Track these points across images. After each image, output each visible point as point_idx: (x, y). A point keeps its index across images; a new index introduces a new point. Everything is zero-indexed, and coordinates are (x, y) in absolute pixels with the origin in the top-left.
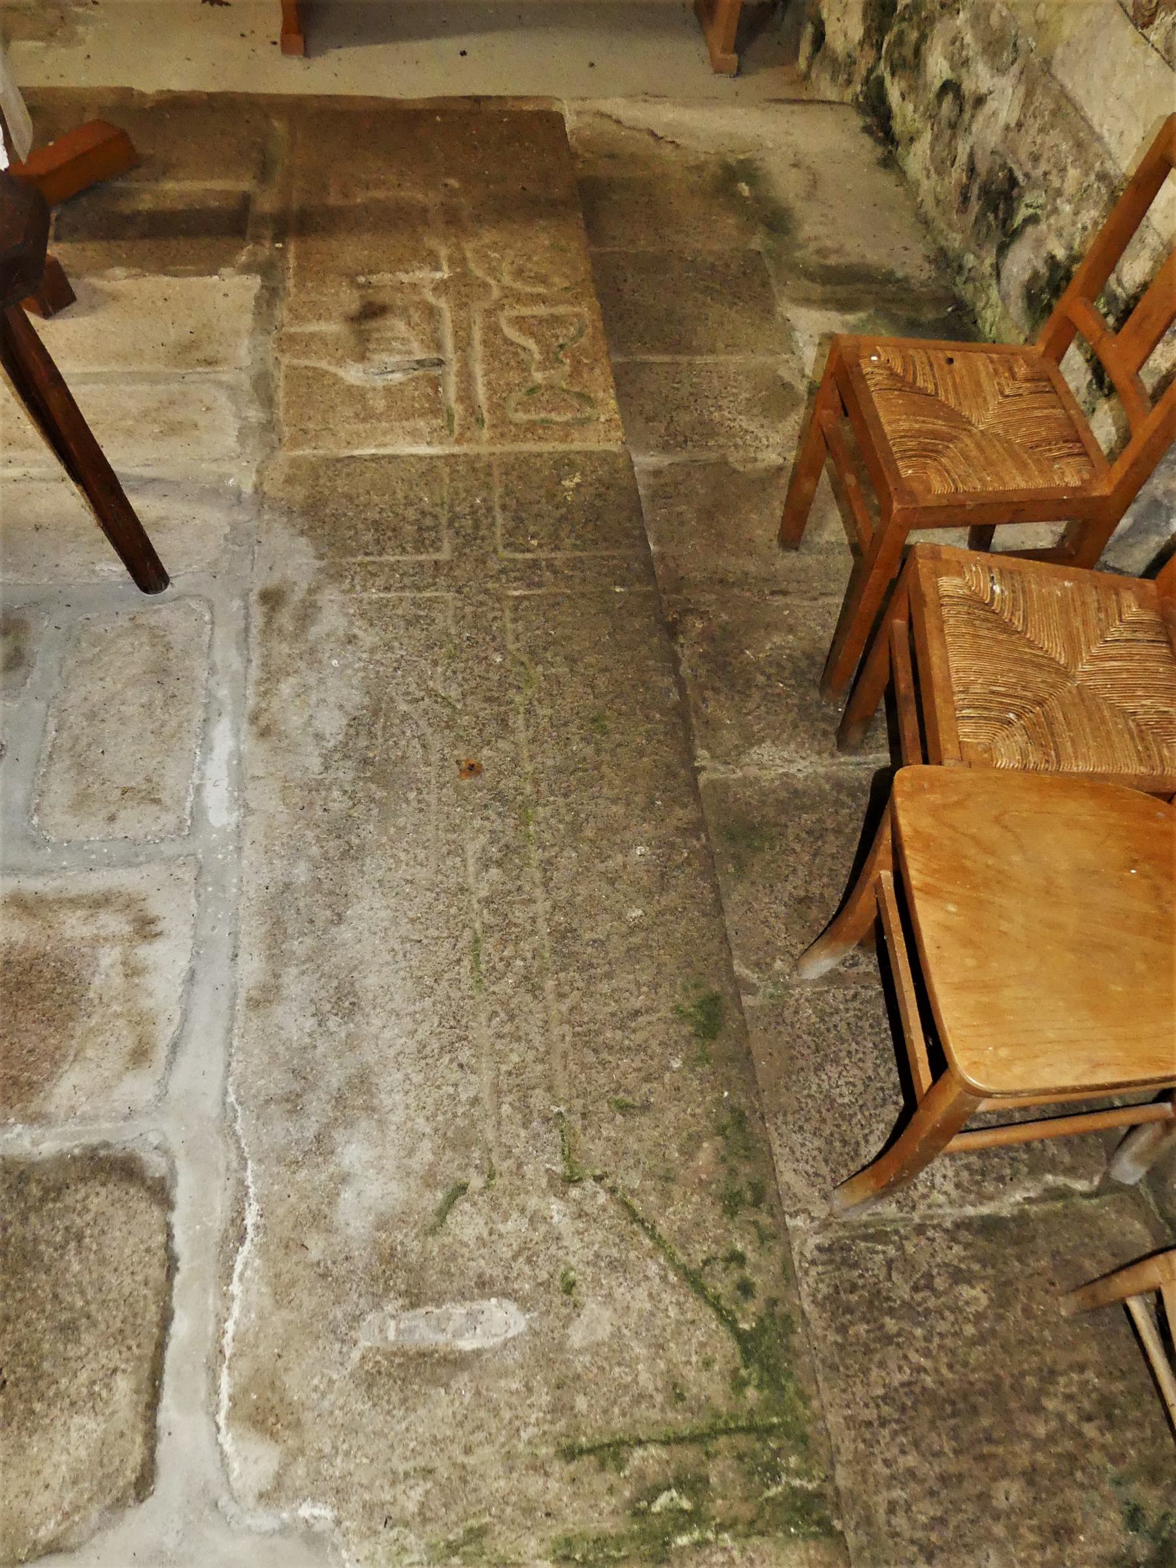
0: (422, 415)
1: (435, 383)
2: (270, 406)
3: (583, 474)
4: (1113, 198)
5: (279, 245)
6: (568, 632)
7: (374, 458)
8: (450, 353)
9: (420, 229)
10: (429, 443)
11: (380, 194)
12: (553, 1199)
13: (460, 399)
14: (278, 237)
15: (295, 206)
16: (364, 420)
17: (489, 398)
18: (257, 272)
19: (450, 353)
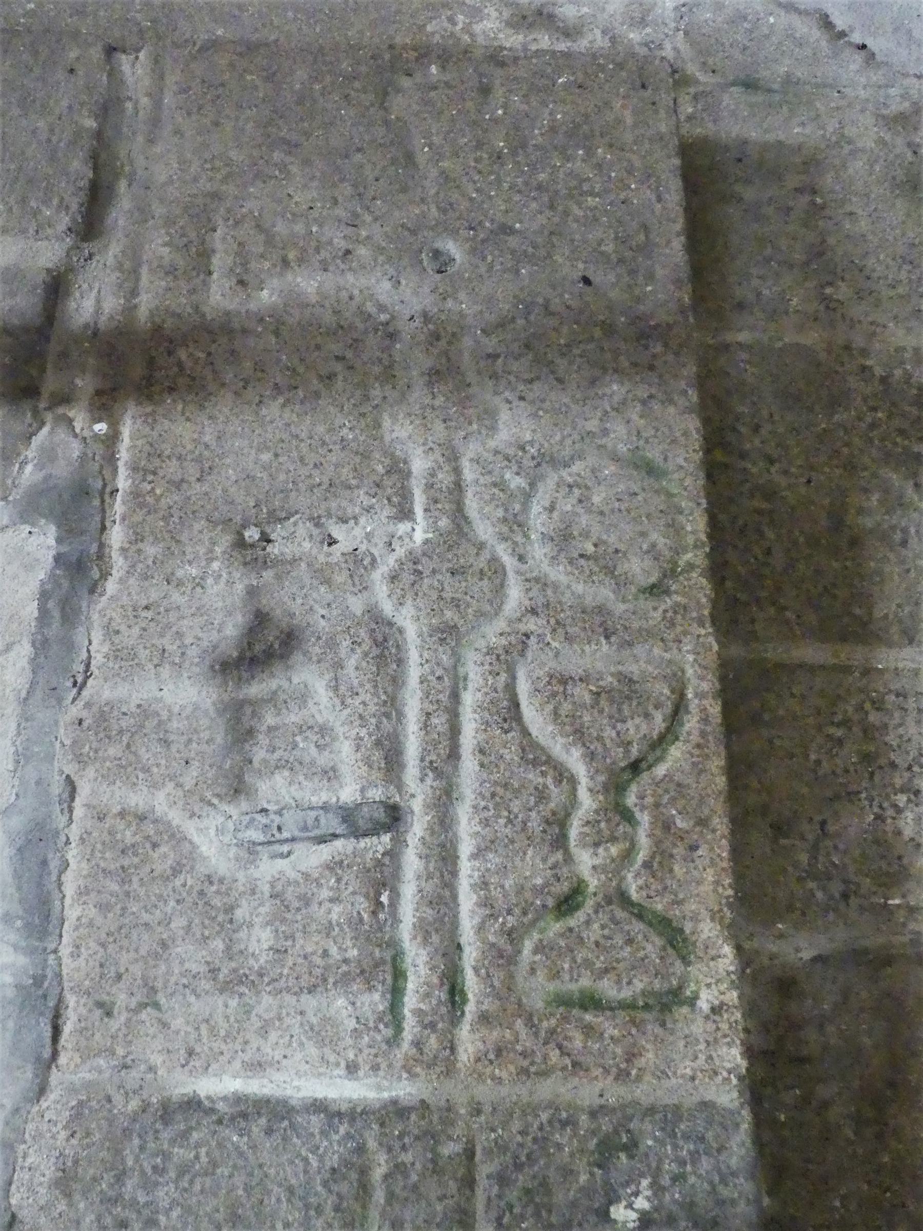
0: (345, 980)
1: (382, 879)
2: (43, 934)
3: (657, 1188)
4: (740, 1078)
5: (101, 427)
6: (906, 425)
7: (246, 1110)
8: (417, 793)
9: (376, 393)
10: (352, 1069)
11: (308, 283)
12: (851, 171)
13: (424, 931)
14: (105, 403)
15: (143, 313)
16: (225, 988)
17: (480, 929)
18: (50, 515)
19: (417, 793)
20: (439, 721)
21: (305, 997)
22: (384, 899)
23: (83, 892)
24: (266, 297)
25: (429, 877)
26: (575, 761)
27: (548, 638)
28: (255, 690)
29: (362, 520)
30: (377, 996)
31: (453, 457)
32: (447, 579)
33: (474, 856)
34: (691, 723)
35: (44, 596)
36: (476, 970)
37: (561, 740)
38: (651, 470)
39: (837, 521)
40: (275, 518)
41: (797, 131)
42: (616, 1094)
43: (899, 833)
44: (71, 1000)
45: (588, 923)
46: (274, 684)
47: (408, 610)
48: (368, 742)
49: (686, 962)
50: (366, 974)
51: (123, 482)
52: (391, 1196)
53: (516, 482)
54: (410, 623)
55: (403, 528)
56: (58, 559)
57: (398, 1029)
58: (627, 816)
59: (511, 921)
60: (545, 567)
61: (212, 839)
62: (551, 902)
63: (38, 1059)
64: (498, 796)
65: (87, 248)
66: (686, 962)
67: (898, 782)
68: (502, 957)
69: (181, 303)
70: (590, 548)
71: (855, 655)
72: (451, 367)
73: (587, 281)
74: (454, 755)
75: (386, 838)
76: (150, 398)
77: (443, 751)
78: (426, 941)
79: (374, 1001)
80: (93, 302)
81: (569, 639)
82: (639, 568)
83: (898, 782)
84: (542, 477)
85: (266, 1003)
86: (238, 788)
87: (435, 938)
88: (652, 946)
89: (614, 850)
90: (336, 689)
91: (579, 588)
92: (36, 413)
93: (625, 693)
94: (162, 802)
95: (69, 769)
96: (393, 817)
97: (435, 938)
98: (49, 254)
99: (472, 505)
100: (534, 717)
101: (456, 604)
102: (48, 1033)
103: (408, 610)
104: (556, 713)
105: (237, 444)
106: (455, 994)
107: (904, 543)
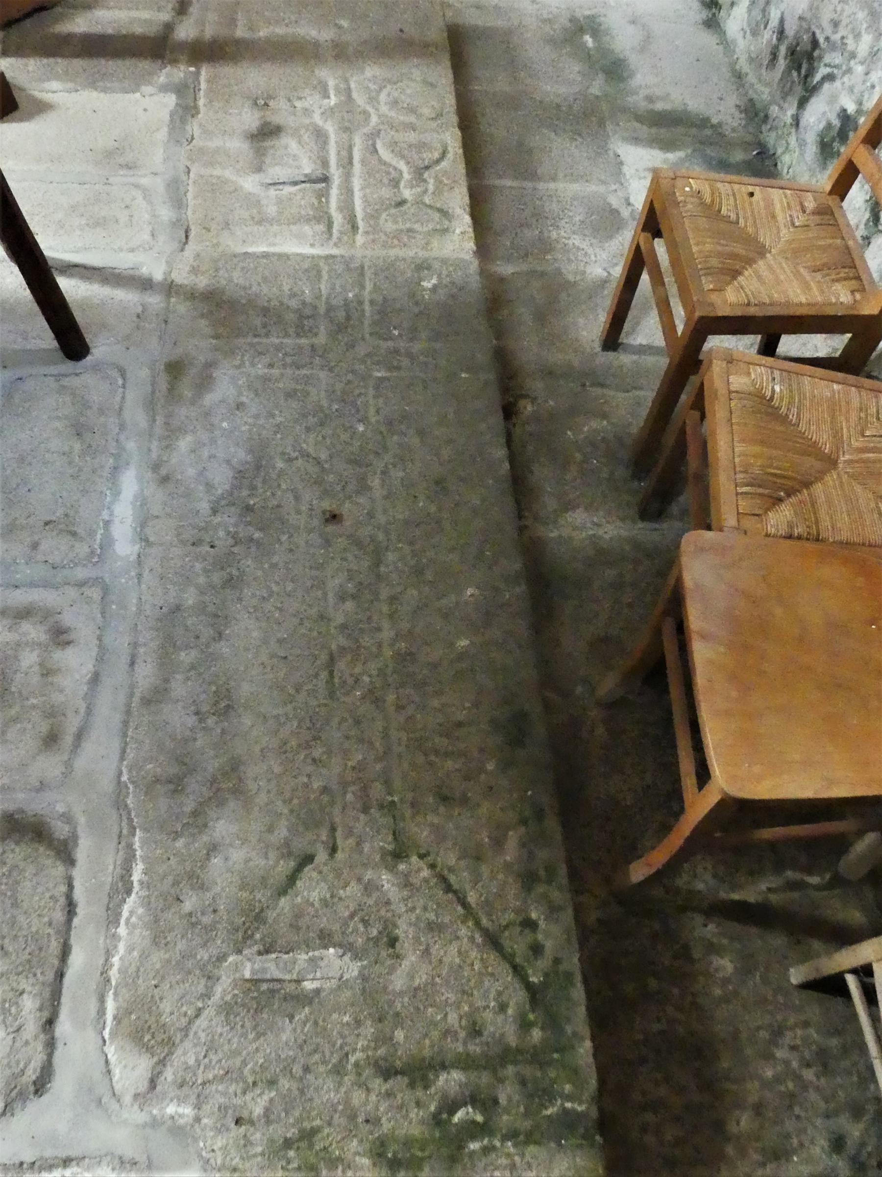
5: (192, 69)
8: (336, 173)
11: (280, 30)
20: (344, 153)
21: (292, 227)
22: (323, 200)
23: (195, 198)
24: (262, 34)
25: (342, 194)
26: (402, 166)
27: (389, 130)
28: (266, 144)
29: (308, 99)
30: (321, 227)
31: (346, 81)
32: (345, 114)
33: (360, 190)
34: (450, 156)
35: (172, 115)
36: (363, 220)
37: (396, 159)
38: (433, 85)
39: (520, 144)
40: (270, 97)
41: (500, 23)
42: (422, 254)
43: (549, 237)
44: (193, 227)
45: (409, 208)
46: (273, 143)
47: (329, 123)
48: (314, 158)
49: (450, 221)
50: (318, 220)
51: (203, 86)
52: (330, 277)
53: (372, 87)
54: (330, 128)
55: (326, 101)
56: (177, 104)
57: (331, 235)
58: (425, 181)
59: (376, 207)
60: (387, 112)
61: (250, 183)
62: (393, 203)
63: (180, 242)
64: (370, 173)
65: (180, 17)
66: (450, 221)
67: (549, 223)
68: (373, 217)
69: (224, 32)
70: (405, 105)
71: (529, 185)
72: (342, 54)
73: (401, 31)
74: (351, 162)
75: (324, 185)
76: (213, 61)
77: (346, 161)
78: (341, 211)
79: (321, 227)
80: (185, 32)
81: (397, 131)
82: (426, 111)
83: (549, 223)
84: (385, 87)
85: (275, 228)
86: (259, 169)
87: (345, 211)
88: (437, 216)
89: (419, 190)
90: (300, 143)
91: (402, 118)
92: (163, 62)
93: (422, 146)
94: (228, 174)
95: (189, 164)
96: (325, 179)
97: (345, 211)
98: (165, 16)
99: (355, 95)
100: (385, 154)
101: (349, 121)
102: (184, 236)
103: (329, 123)
104: (393, 151)
105: (254, 77)
106: (354, 227)
107: (550, 151)
